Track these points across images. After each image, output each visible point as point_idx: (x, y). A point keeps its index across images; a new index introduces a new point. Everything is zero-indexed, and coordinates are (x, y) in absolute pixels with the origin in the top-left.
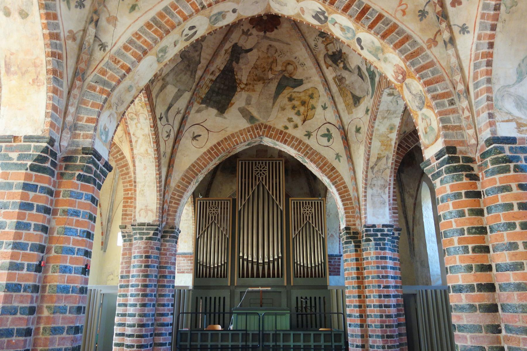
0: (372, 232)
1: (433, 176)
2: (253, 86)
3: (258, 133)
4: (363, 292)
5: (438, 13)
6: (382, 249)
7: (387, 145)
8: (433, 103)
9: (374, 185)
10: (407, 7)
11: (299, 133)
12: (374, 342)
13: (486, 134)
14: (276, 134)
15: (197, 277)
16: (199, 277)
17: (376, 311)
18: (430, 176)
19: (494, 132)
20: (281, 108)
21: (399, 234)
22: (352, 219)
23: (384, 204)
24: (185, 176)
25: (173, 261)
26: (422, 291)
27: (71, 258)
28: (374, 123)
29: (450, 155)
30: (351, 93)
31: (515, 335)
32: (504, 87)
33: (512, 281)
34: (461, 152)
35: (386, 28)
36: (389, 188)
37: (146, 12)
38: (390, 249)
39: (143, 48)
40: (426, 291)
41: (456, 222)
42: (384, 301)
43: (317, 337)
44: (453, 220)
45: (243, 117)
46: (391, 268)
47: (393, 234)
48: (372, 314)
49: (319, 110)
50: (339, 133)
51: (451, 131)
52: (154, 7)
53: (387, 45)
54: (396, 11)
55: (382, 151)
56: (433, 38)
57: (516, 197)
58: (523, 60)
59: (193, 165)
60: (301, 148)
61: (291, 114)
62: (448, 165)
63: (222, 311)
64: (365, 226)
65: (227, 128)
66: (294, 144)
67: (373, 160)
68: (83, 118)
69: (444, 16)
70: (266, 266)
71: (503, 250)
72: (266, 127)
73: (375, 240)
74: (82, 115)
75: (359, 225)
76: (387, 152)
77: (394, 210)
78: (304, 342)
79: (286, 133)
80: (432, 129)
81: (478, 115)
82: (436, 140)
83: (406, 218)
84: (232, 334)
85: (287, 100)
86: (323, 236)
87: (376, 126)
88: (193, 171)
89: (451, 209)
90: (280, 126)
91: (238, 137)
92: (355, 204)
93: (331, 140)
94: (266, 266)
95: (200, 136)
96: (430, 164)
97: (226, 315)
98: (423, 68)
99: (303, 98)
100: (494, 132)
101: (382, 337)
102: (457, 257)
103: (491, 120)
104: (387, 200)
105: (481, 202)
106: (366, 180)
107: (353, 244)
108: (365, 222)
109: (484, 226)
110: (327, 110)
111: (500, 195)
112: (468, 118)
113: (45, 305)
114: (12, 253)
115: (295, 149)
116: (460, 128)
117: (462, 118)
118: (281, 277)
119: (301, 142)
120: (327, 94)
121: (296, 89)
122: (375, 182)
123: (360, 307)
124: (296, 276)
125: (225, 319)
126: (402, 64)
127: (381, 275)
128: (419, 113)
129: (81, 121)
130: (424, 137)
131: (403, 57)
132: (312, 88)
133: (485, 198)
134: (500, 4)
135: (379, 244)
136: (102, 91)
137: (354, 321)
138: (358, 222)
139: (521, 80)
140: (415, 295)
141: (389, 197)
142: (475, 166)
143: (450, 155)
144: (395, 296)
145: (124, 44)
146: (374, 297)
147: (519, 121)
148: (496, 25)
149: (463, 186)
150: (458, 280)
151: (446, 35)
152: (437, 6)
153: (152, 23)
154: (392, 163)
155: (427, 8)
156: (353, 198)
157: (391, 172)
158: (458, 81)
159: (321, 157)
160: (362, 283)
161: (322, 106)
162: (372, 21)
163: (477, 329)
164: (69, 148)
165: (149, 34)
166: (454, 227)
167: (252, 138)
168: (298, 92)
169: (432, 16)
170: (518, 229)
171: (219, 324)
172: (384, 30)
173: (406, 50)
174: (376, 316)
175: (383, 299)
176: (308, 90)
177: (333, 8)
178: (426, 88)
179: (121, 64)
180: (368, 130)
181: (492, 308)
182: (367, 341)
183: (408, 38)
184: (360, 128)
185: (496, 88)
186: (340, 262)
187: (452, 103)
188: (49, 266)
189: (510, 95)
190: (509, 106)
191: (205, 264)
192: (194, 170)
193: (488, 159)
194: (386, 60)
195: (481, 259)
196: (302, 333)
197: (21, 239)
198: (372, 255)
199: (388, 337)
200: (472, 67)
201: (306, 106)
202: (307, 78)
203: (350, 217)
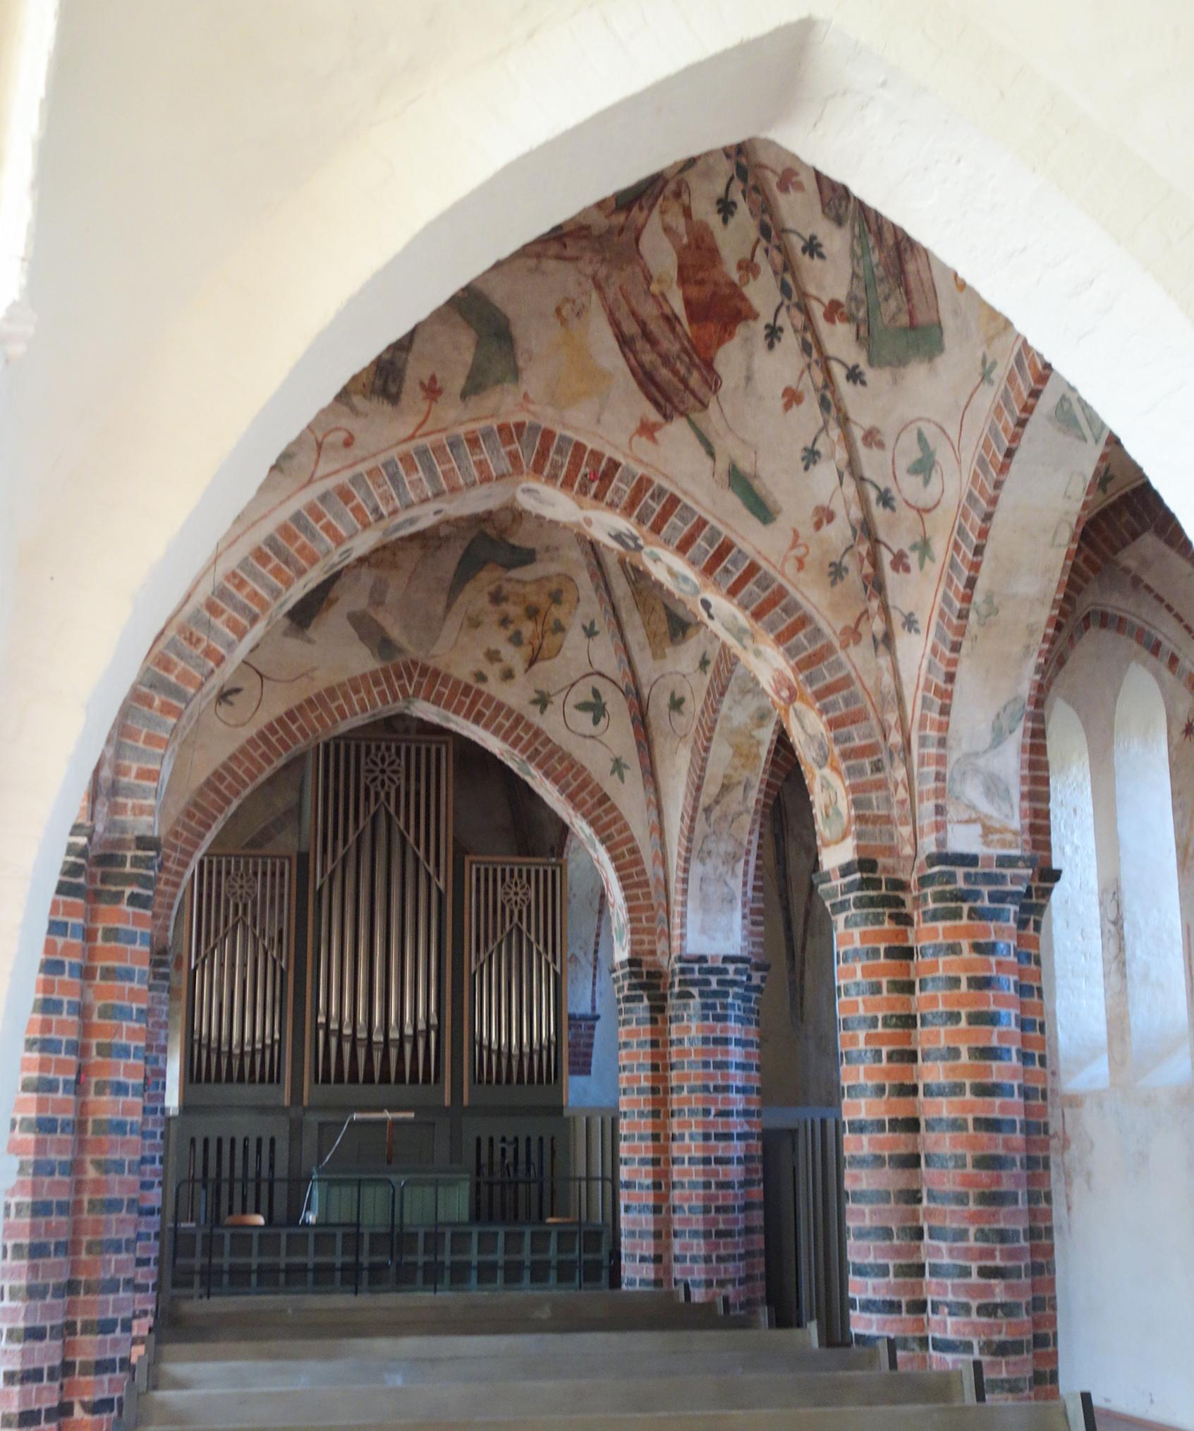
0: (697, 976)
1: (833, 906)
2: (394, 554)
3: (403, 688)
4: (664, 1126)
5: (866, 577)
6: (717, 1018)
7: (747, 757)
8: (843, 767)
9: (709, 853)
10: (808, 552)
11: (515, 695)
12: (685, 1247)
13: (929, 845)
14: (453, 695)
15: (191, 1081)
16: (199, 1080)
17: (696, 1173)
18: (828, 904)
19: (941, 843)
20: (470, 619)
21: (763, 979)
22: (646, 938)
23: (731, 901)
24: (196, 804)
25: (162, 1042)
26: (813, 1122)
27: (126, 1066)
28: (719, 702)
29: (865, 875)
30: (666, 607)
31: (940, 1206)
32: (968, 755)
33: (945, 1114)
34: (885, 869)
35: (764, 595)
36: (747, 863)
37: (254, 524)
38: (738, 1019)
39: (250, 611)
40: (823, 1122)
41: (864, 1002)
42: (715, 1148)
43: (540, 1240)
44: (860, 999)
45: (361, 638)
46: (738, 1066)
47: (749, 978)
48: (686, 1180)
49: (575, 635)
50: (625, 705)
51: (870, 827)
52: (270, 512)
53: (763, 632)
54: (785, 559)
55: (736, 769)
56: (853, 625)
57: (967, 966)
58: (1005, 709)
59: (217, 775)
60: (519, 738)
61: (498, 640)
62: (859, 894)
63: (265, 1173)
64: (680, 959)
65: (314, 669)
66: (500, 726)
67: (710, 789)
68: (129, 769)
69: (876, 585)
70: (393, 1052)
71: (936, 1059)
72: (424, 671)
73: (702, 994)
74: (126, 763)
75: (663, 953)
76: (746, 773)
77: (755, 916)
78: (506, 1252)
79: (479, 693)
80: (838, 813)
81: (921, 801)
82: (844, 837)
83: (786, 909)
84: (317, 1236)
85: (486, 598)
86: (558, 970)
87: (724, 708)
88: (218, 792)
89: (859, 976)
90: (463, 672)
91: (346, 697)
92: (657, 899)
93: (603, 722)
94: (393, 1052)
95: (237, 691)
96: (830, 880)
97: (277, 1186)
98: (830, 689)
99: (533, 599)
100: (941, 843)
101: (707, 1235)
102: (862, 1068)
103: (939, 818)
104: (739, 894)
105: (912, 968)
106: (690, 840)
107: (646, 1002)
108: (681, 948)
109: (913, 1013)
110: (597, 638)
111: (941, 960)
112: (903, 802)
113: (88, 1158)
114: (42, 1059)
115: (505, 739)
116: (888, 820)
117: (894, 800)
118: (436, 1081)
119: (519, 719)
120: (601, 600)
121: (515, 574)
122: (711, 845)
123: (655, 1162)
124: (477, 1080)
125: (276, 1199)
126: (789, 673)
127: (711, 1085)
128: (818, 772)
129: (125, 775)
130: (825, 823)
131: (792, 663)
132: (559, 575)
133: (918, 959)
134: (968, 611)
135: (713, 1007)
136: (167, 709)
137: (640, 1198)
138: (661, 946)
139: (999, 743)
140: (793, 1133)
141: (745, 884)
142: (908, 898)
143: (865, 875)
144: (741, 1137)
145: (208, 599)
146: (692, 1137)
147: (989, 823)
148: (961, 644)
149: (882, 936)
150: (859, 1110)
151: (878, 626)
152: (866, 562)
153: (267, 550)
154: (758, 801)
155: (847, 561)
156: (652, 882)
157: (754, 822)
158: (893, 724)
159: (572, 767)
160: (664, 1102)
161: (584, 628)
162: (735, 577)
163: (883, 1197)
164: (107, 835)
165: (262, 576)
166: (861, 1011)
167: (385, 701)
168: (518, 581)
169: (854, 577)
170: (963, 1024)
171: (257, 1211)
172: (759, 601)
173: (798, 648)
174: (693, 1185)
175: (713, 1142)
176: (548, 579)
177: (657, 538)
178: (832, 735)
179: (203, 645)
180: (703, 713)
181: (911, 1161)
182: (669, 1247)
183: (804, 621)
184: (681, 701)
185: (953, 756)
186: (592, 1036)
187: (877, 767)
188: (89, 1083)
189: (977, 771)
190: (973, 792)
191: (214, 1045)
192: (222, 788)
193: (929, 891)
194: (758, 653)
195: (900, 1072)
196: (501, 1231)
197: (50, 1031)
198: (693, 1033)
199: (720, 1234)
200: (919, 702)
201: (540, 620)
202: (547, 549)
203: (643, 931)
